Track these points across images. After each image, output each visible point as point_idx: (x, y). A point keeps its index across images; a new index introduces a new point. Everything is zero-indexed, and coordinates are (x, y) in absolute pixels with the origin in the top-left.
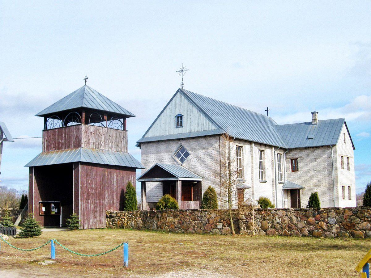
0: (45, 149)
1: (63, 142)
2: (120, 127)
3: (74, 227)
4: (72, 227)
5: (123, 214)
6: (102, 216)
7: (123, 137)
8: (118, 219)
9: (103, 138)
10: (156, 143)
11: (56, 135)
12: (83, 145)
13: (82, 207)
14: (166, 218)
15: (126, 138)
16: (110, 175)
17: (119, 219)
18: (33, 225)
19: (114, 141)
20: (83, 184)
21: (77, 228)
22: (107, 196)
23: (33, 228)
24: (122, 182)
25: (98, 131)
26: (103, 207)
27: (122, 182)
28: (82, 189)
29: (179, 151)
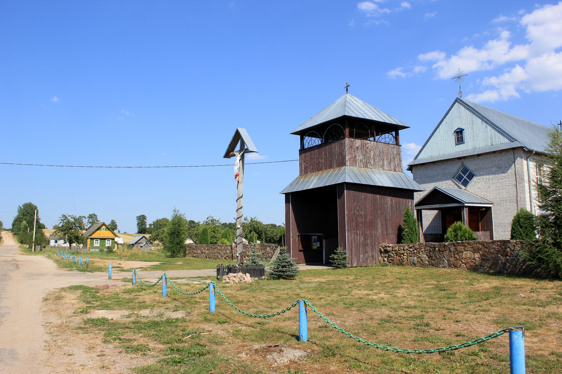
0: (303, 172)
1: (324, 161)
2: (393, 141)
3: (339, 265)
4: (338, 264)
5: (402, 248)
6: (374, 251)
7: (395, 153)
8: (395, 255)
9: (372, 154)
10: (431, 165)
11: (314, 154)
12: (348, 163)
13: (350, 239)
14: (463, 253)
15: (399, 155)
16: (382, 200)
17: (396, 254)
18: (286, 262)
19: (385, 158)
20: (350, 211)
21: (345, 266)
22: (379, 226)
23: (286, 267)
24: (398, 208)
25: (366, 146)
26: (375, 240)
27: (398, 208)
28: (348, 217)
29: (460, 172)
